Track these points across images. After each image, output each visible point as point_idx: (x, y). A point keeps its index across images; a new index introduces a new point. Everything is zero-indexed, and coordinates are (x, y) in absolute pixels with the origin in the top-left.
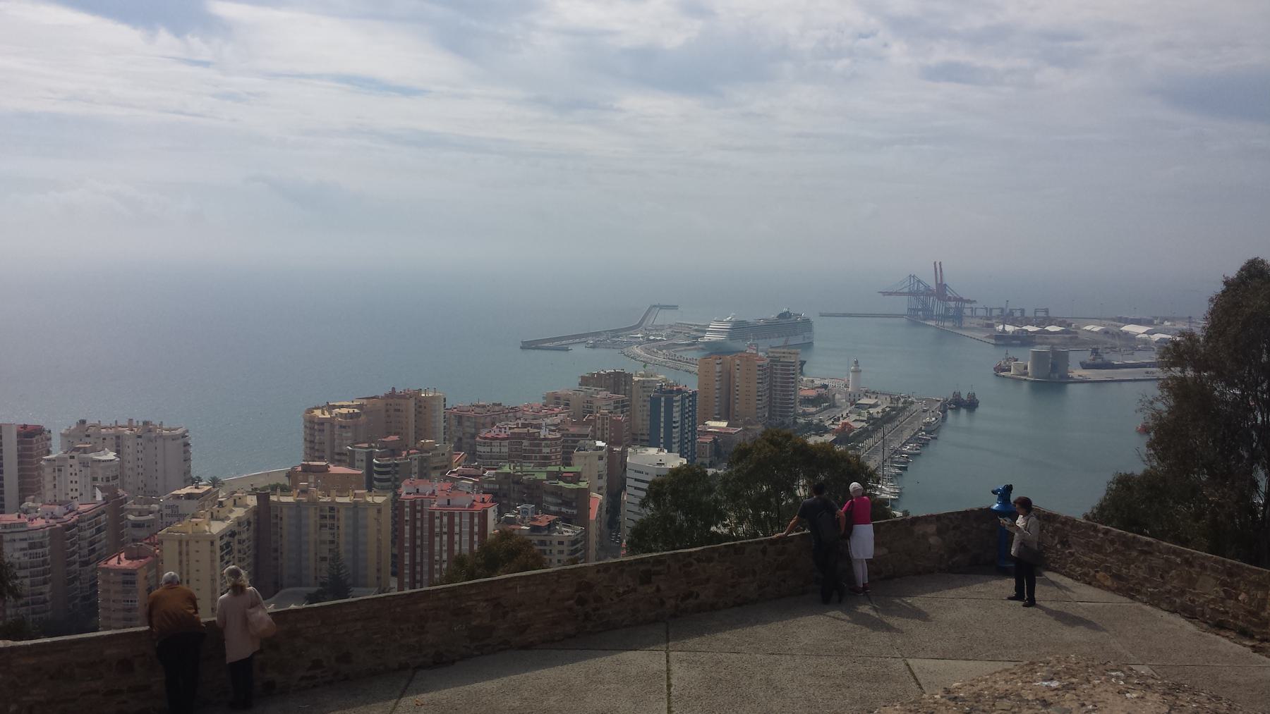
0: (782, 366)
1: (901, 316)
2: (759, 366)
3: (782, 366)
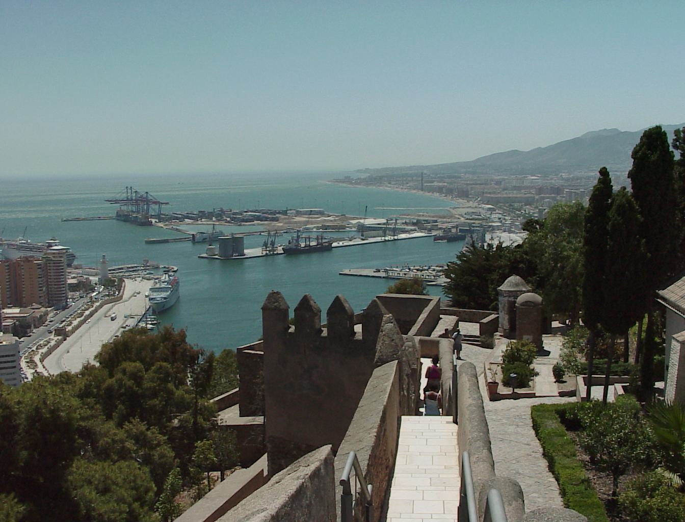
0: (54, 263)
1: (111, 218)
2: (38, 265)
3: (54, 263)
